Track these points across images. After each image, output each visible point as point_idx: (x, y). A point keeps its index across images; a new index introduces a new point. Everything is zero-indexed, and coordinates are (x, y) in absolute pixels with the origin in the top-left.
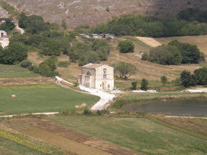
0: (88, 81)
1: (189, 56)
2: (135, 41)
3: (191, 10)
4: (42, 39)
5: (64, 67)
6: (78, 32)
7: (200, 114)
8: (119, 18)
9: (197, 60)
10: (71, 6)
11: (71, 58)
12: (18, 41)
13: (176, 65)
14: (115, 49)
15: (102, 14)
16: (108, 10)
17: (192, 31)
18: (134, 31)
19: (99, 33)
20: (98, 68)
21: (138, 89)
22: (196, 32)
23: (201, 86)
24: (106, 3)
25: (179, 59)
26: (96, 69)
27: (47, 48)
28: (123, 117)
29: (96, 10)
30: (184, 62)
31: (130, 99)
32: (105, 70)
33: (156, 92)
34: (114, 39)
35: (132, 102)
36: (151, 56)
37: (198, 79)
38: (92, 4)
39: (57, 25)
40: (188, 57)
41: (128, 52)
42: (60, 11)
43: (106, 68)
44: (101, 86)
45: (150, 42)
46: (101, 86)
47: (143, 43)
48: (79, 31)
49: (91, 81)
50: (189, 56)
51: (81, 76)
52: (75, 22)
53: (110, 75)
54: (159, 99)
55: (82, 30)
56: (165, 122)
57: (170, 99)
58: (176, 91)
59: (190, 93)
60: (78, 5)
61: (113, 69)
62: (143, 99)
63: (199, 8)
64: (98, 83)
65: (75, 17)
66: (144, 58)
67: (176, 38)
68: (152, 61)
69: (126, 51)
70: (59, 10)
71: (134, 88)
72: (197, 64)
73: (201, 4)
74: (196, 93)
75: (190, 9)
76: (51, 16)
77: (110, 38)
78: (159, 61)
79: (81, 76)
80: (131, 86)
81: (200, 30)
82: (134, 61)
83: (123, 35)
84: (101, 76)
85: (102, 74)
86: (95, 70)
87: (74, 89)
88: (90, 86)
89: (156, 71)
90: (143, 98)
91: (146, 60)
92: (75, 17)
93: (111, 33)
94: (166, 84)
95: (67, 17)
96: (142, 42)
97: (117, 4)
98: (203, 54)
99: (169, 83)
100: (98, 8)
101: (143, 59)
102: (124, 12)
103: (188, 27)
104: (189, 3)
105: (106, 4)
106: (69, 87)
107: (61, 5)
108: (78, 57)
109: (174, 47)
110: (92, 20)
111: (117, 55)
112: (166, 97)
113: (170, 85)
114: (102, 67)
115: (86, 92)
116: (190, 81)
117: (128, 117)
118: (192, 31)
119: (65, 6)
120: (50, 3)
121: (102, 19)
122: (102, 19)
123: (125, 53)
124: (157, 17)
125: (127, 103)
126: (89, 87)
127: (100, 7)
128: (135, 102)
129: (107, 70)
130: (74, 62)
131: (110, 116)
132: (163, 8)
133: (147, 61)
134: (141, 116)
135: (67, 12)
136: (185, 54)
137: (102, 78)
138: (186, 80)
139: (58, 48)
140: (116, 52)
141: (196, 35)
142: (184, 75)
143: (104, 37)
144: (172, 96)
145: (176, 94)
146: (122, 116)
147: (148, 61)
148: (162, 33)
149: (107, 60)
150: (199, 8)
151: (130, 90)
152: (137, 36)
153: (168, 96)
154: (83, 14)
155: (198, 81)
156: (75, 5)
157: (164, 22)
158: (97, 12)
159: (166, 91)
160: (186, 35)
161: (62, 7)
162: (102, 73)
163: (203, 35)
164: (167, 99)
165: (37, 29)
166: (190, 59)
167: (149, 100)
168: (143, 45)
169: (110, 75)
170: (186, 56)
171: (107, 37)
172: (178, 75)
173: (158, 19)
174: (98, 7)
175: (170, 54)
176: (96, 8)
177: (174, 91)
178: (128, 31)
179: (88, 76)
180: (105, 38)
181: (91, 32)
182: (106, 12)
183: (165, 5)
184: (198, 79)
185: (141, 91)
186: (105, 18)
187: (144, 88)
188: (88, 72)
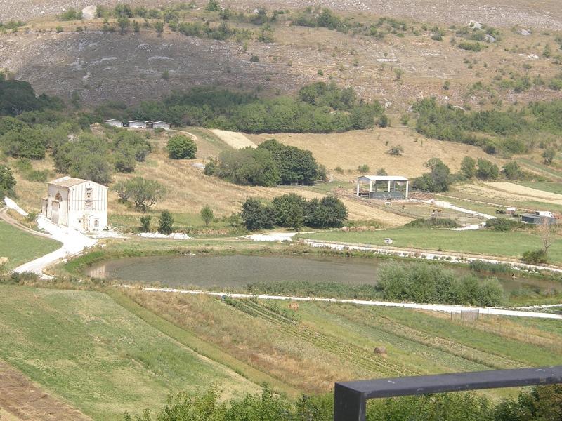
0: (57, 210)
1: (295, 170)
2: (208, 136)
3: (321, 86)
4: (14, 126)
5: (38, 181)
6: (102, 116)
7: (215, 286)
8: (186, 93)
9: (311, 179)
10: (97, 66)
11: (57, 165)
12: (30, 120)
13: (267, 186)
14: (160, 150)
15: (153, 84)
16: (165, 77)
17: (318, 123)
18: (209, 118)
19: (141, 120)
20: (74, 187)
21: (153, 231)
22: (326, 127)
23: (283, 229)
24: (166, 64)
25: (273, 175)
26: (70, 188)
27: (18, 144)
28: (60, 289)
29: (143, 76)
30: (286, 182)
31: (121, 250)
32: (89, 192)
33: (188, 237)
34: (169, 132)
35: (124, 256)
36: (222, 167)
37: (278, 216)
38: (136, 64)
39: (62, 101)
40: (293, 173)
41: (182, 157)
42: (74, 75)
43: (91, 187)
44: (80, 222)
45: (237, 140)
46: (80, 222)
47: (223, 141)
48: (103, 114)
49: (61, 211)
50: (295, 170)
51: (47, 200)
52: (99, 97)
53: (100, 201)
54: (181, 251)
55: (110, 112)
56: (137, 304)
57: (204, 252)
58: (229, 236)
59: (252, 242)
60: (110, 64)
61: (107, 190)
62: (148, 252)
63: (338, 83)
64: (75, 215)
65: (99, 86)
66: (209, 171)
67: (273, 136)
68: (221, 177)
69: (178, 155)
70: (72, 73)
71: (145, 229)
72: (310, 187)
73: (343, 76)
74: (262, 242)
75: (320, 83)
76: (54, 83)
77: (162, 130)
78: (234, 177)
79: (47, 200)
80: (139, 225)
81: (333, 123)
82: (188, 174)
83: (189, 124)
84: (80, 202)
85: (84, 199)
86: (69, 191)
87: (24, 225)
88: (60, 222)
89: (219, 196)
90: (152, 249)
91: (211, 174)
92: (99, 86)
93: (164, 120)
94: (211, 223)
95: (85, 87)
96: (221, 140)
97: (186, 67)
98: (323, 167)
99: (216, 221)
100: (148, 73)
101: (206, 173)
102: (198, 83)
103: (311, 117)
104: (320, 73)
105: (165, 66)
106: (16, 222)
107: (77, 63)
108: (70, 163)
109: (266, 152)
110: (133, 95)
111: (161, 162)
112: (197, 248)
113: (219, 224)
114: (84, 186)
115: (39, 230)
116: (259, 219)
117: (71, 289)
118: (318, 123)
119: (84, 66)
120: (58, 60)
121: (152, 94)
122: (152, 94)
123: (178, 159)
124: (256, 96)
125: (110, 258)
126: (57, 223)
127: (152, 71)
128: (130, 256)
129: (94, 191)
130: (63, 172)
131: (37, 286)
132: (272, 78)
133: (212, 177)
134: (97, 287)
135: (86, 77)
136: (289, 165)
137: (83, 206)
138: (252, 217)
139: (39, 143)
140: (162, 156)
141: (326, 132)
142: (249, 206)
143: (152, 127)
144: (209, 248)
145: (222, 243)
146: (60, 285)
147: (215, 176)
148: (262, 126)
149: (134, 171)
150: (338, 83)
151: (136, 233)
152: (215, 128)
153: (202, 247)
154: (115, 81)
155: (279, 219)
156: (104, 64)
157: (268, 105)
158: (143, 81)
159: (207, 237)
160: (307, 131)
161: (79, 68)
162: (84, 197)
163: (340, 132)
164: (197, 252)
165: (15, 105)
166: (296, 177)
167: (160, 253)
168: (221, 143)
169: (100, 201)
170: (289, 169)
171: (155, 126)
172: (455, 190)
173: (258, 99)
174: (148, 72)
175: (257, 166)
176: (145, 71)
177: (224, 236)
178: (199, 118)
179: (57, 201)
180: (152, 129)
181: (128, 117)
182: (162, 80)
183: (277, 74)
184: (278, 216)
185: (158, 235)
186: (159, 92)
187: (165, 228)
188: (58, 194)
